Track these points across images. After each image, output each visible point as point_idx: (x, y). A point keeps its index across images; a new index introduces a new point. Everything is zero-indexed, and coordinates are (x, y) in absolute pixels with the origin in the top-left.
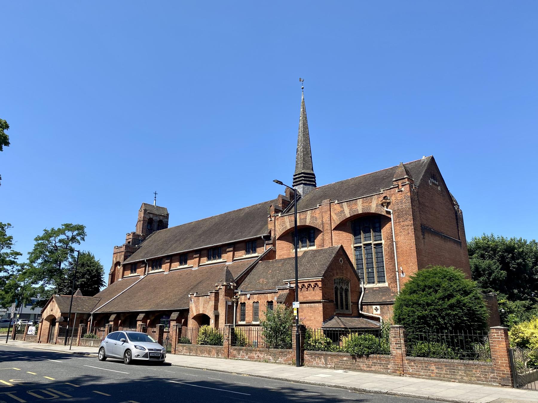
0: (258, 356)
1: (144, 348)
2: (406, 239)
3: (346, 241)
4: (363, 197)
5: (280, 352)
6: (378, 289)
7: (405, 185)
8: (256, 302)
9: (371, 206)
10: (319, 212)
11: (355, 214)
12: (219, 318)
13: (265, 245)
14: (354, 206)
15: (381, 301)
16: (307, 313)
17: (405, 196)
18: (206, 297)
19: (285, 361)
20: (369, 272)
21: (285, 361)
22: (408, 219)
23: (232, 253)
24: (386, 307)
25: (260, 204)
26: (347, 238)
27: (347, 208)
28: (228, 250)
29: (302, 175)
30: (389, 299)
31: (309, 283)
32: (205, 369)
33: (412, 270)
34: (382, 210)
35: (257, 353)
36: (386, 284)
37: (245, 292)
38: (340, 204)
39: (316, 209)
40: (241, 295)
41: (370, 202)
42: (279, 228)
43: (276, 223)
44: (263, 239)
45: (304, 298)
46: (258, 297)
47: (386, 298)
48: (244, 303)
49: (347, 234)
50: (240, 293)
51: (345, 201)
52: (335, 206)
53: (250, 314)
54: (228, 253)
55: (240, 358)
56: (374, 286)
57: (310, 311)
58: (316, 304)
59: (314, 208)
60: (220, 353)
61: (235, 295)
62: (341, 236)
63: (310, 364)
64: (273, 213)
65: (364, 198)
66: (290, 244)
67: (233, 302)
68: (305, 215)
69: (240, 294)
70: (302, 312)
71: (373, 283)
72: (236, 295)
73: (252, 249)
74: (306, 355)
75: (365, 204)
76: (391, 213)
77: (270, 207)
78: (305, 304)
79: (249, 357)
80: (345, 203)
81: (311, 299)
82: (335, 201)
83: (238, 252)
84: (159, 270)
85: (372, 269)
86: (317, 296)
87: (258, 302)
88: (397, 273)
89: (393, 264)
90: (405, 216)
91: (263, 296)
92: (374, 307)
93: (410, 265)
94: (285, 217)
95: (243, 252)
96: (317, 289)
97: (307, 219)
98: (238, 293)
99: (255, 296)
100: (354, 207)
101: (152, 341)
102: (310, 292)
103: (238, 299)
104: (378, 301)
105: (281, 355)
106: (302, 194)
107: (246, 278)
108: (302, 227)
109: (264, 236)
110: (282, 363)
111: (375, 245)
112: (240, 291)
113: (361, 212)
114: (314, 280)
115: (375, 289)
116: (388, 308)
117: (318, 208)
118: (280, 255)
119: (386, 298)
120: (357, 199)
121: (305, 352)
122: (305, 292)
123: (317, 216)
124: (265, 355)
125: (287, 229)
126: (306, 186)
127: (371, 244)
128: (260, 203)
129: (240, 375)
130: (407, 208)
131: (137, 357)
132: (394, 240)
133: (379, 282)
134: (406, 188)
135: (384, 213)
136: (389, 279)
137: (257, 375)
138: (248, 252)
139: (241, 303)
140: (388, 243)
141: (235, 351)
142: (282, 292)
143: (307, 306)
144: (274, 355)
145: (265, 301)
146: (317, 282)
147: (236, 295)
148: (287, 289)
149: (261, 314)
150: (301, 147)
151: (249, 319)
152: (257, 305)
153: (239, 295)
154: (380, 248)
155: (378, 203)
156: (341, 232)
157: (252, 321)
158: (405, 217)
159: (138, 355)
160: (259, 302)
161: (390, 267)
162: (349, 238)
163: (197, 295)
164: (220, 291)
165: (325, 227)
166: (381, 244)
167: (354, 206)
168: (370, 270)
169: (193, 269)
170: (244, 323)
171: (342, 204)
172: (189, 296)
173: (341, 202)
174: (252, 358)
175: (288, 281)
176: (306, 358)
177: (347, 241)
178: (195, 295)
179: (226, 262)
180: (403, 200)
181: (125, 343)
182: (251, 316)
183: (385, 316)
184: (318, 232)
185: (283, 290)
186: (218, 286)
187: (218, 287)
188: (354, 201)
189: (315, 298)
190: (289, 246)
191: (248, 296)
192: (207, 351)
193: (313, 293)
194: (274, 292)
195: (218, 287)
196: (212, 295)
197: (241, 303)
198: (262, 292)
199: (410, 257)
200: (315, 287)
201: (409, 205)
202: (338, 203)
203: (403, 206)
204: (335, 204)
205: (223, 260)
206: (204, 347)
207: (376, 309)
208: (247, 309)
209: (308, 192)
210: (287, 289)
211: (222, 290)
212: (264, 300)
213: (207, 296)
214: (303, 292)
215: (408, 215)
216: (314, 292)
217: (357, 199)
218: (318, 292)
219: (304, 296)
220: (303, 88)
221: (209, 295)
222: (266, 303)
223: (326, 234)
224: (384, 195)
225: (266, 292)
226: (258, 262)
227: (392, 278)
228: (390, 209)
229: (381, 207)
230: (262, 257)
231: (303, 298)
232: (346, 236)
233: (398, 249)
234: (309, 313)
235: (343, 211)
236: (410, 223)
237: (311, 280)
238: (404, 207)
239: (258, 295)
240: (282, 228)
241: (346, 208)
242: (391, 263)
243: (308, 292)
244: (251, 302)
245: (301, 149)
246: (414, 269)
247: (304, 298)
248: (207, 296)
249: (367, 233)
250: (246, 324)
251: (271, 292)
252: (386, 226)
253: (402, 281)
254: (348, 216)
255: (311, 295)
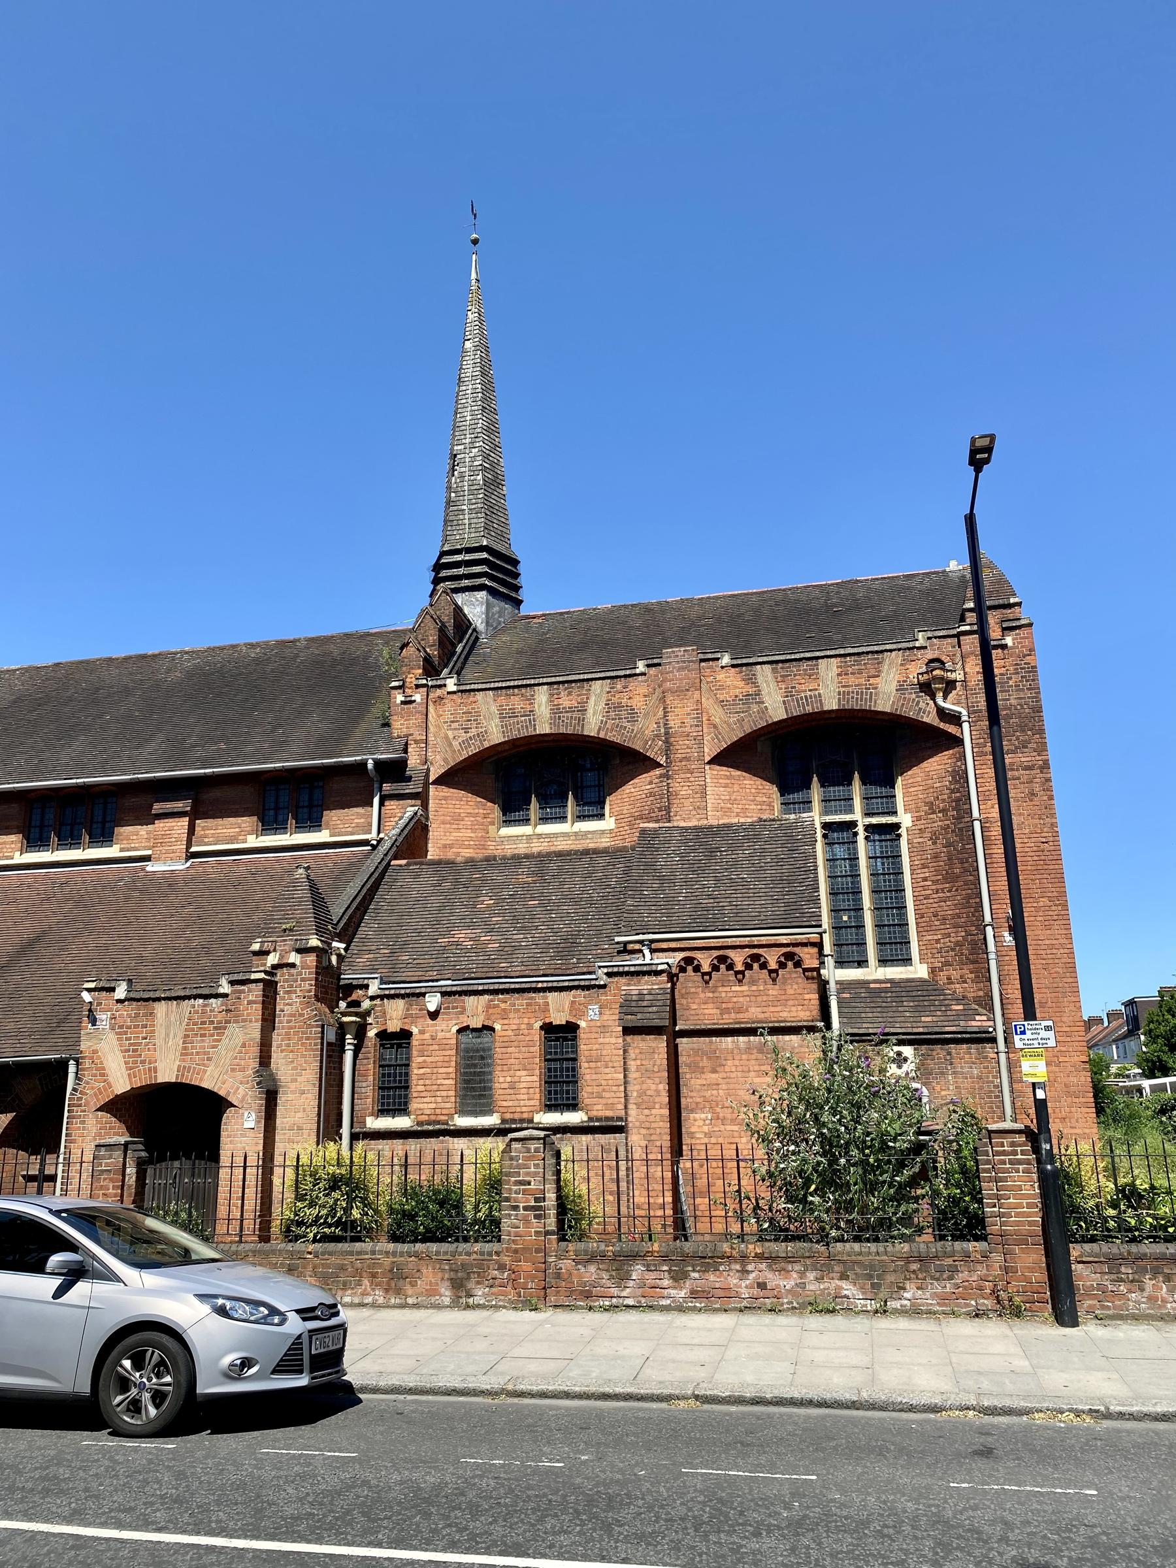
0: (762, 1286)
1: (274, 1311)
2: (1023, 814)
3: (753, 807)
4: (842, 652)
5: (908, 1259)
6: (889, 985)
7: (1019, 627)
8: (475, 1030)
9: (876, 688)
10: (643, 690)
11: (809, 709)
12: (276, 1105)
13: (376, 800)
14: (803, 681)
15: (921, 1030)
16: (739, 1074)
17: (1017, 664)
18: (201, 1001)
19: (943, 1299)
20: (843, 925)
21: (943, 1299)
22: (1030, 746)
23: (184, 822)
24: (939, 1051)
25: (252, 646)
26: (758, 799)
27: (773, 685)
28: (157, 807)
29: (485, 555)
30: (951, 1024)
31: (755, 951)
32: (685, 1398)
33: (1047, 923)
34: (922, 705)
35: (750, 1267)
36: (919, 970)
37: (394, 983)
38: (744, 668)
39: (631, 679)
40: (382, 997)
41: (873, 672)
42: (447, 737)
43: (430, 716)
44: (372, 774)
45: (724, 1011)
46: (488, 1006)
47: (935, 1019)
48: (405, 1035)
49: (759, 781)
50: (374, 989)
51: (765, 659)
52: (721, 676)
53: (439, 1082)
54: (160, 825)
55: (630, 1302)
56: (869, 974)
57: (757, 1068)
58: (787, 1038)
59: (622, 673)
60: (478, 1283)
61: (344, 999)
62: (736, 787)
63: (1108, 1308)
64: (414, 675)
65: (848, 658)
66: (489, 804)
67: (342, 1029)
68: (578, 695)
69: (380, 992)
70: (714, 1071)
71: (862, 963)
72: (354, 997)
73: (60, 829)
74: (1081, 1266)
75: (852, 680)
76: (964, 718)
77: (402, 649)
78: (729, 1039)
79: (694, 1294)
80: (767, 667)
81: (762, 1016)
82: (719, 655)
83: (220, 821)
84: (56, 853)
85: (852, 913)
86: (791, 1003)
87: (493, 1029)
88: (989, 930)
89: (959, 898)
90: (1018, 734)
91: (520, 1001)
92: (891, 1051)
93: (1041, 904)
94: (480, 695)
95: (15, 839)
96: (794, 975)
97: (590, 711)
98: (367, 987)
99: (471, 1001)
100: (803, 687)
101: (187, 1251)
102: (754, 988)
103: (368, 1013)
104: (910, 1030)
105: (914, 1271)
106: (481, 627)
107: (359, 926)
108: (553, 741)
109: (377, 763)
110: (929, 1312)
111: (868, 828)
112: (377, 982)
113: (835, 707)
114: (784, 940)
115: (878, 986)
116: (949, 1054)
117: (643, 674)
118: (445, 846)
119: (935, 1019)
120: (817, 658)
121: (1075, 1251)
122: (728, 989)
123: (638, 702)
124: (811, 1276)
125: (486, 745)
126: (495, 601)
127: (853, 824)
128: (254, 641)
129: (932, 1416)
130: (1025, 707)
131: (239, 1378)
132: (976, 814)
133: (883, 962)
134: (1021, 638)
135: (931, 718)
136: (935, 951)
137: (1159, 1409)
138: (271, 824)
139: (383, 1035)
140: (936, 825)
141: (592, 1268)
142: (629, 985)
143: (742, 1046)
144: (870, 1277)
145: (530, 1026)
146: (797, 950)
147: (354, 997)
148: (658, 973)
149: (509, 1079)
150: (473, 450)
151: (433, 1106)
152: (479, 1040)
153: (372, 998)
154: (888, 843)
155: (906, 681)
156: (739, 773)
157: (451, 1116)
158: (1018, 739)
159: (246, 1363)
160: (497, 1027)
161: (939, 909)
162: (765, 799)
163: (132, 995)
164: (281, 976)
165: (677, 747)
166: (897, 826)
167: (803, 681)
168: (845, 918)
169: (151, 867)
170: (402, 1123)
171: (750, 668)
172: (87, 997)
173: (751, 660)
174: (720, 1293)
175: (641, 942)
176: (1081, 1278)
177: (759, 807)
178: (121, 992)
179: (147, 859)
180: (1010, 678)
181: (82, 1289)
182: (444, 1094)
183: (938, 1083)
184: (631, 767)
185: (635, 979)
186: (267, 953)
187: (272, 959)
188: (805, 665)
189: (785, 1014)
190: (481, 811)
191: (433, 1002)
192: (374, 1276)
193: (773, 991)
194: (587, 983)
195: (272, 959)
196: (243, 991)
197: (383, 1035)
198: (513, 986)
199: (1039, 877)
200: (680, 972)
201: (1033, 697)
202: (733, 666)
203: (1008, 700)
204: (722, 667)
205: (122, 850)
206: (351, 1253)
207: (900, 1060)
208: (425, 1062)
209: (499, 623)
210: (658, 973)
211: (293, 971)
212: (526, 1021)
213: (206, 997)
214: (720, 989)
215: (1029, 733)
216: (777, 987)
217: (817, 658)
218: (795, 986)
219: (724, 1006)
220: (475, 242)
221: (225, 996)
222: (536, 1035)
223: (683, 776)
224: (930, 655)
225: (540, 985)
226: (389, 864)
227: (953, 950)
228: (958, 703)
229: (917, 697)
230: (398, 844)
231: (718, 1011)
232: (753, 791)
233: (994, 847)
234: (752, 1074)
235: (755, 696)
236: (1040, 758)
237: (764, 941)
238: (1013, 702)
239: (486, 997)
240: (464, 736)
241: (768, 686)
242: (948, 894)
243: (745, 988)
244: (447, 1028)
245: (473, 459)
246: (1056, 917)
247: (724, 1011)
248: (213, 1001)
249: (834, 786)
250: (416, 1128)
251: (566, 984)
252: (924, 765)
253: (1007, 958)
254: (778, 713)
255: (759, 999)
